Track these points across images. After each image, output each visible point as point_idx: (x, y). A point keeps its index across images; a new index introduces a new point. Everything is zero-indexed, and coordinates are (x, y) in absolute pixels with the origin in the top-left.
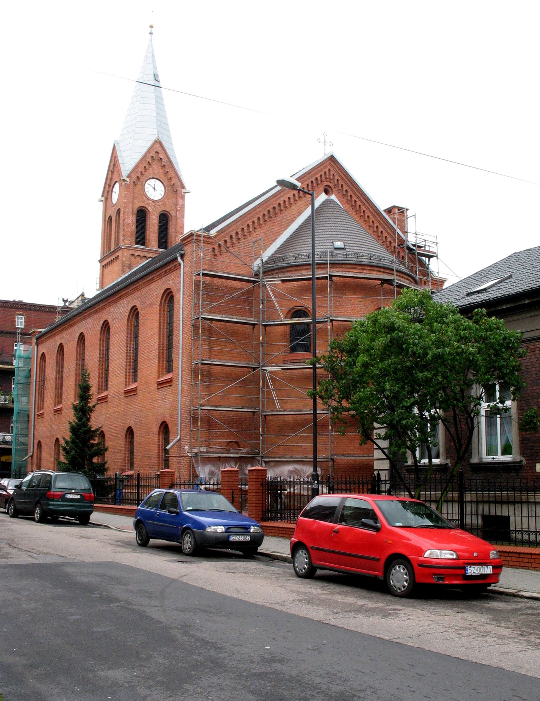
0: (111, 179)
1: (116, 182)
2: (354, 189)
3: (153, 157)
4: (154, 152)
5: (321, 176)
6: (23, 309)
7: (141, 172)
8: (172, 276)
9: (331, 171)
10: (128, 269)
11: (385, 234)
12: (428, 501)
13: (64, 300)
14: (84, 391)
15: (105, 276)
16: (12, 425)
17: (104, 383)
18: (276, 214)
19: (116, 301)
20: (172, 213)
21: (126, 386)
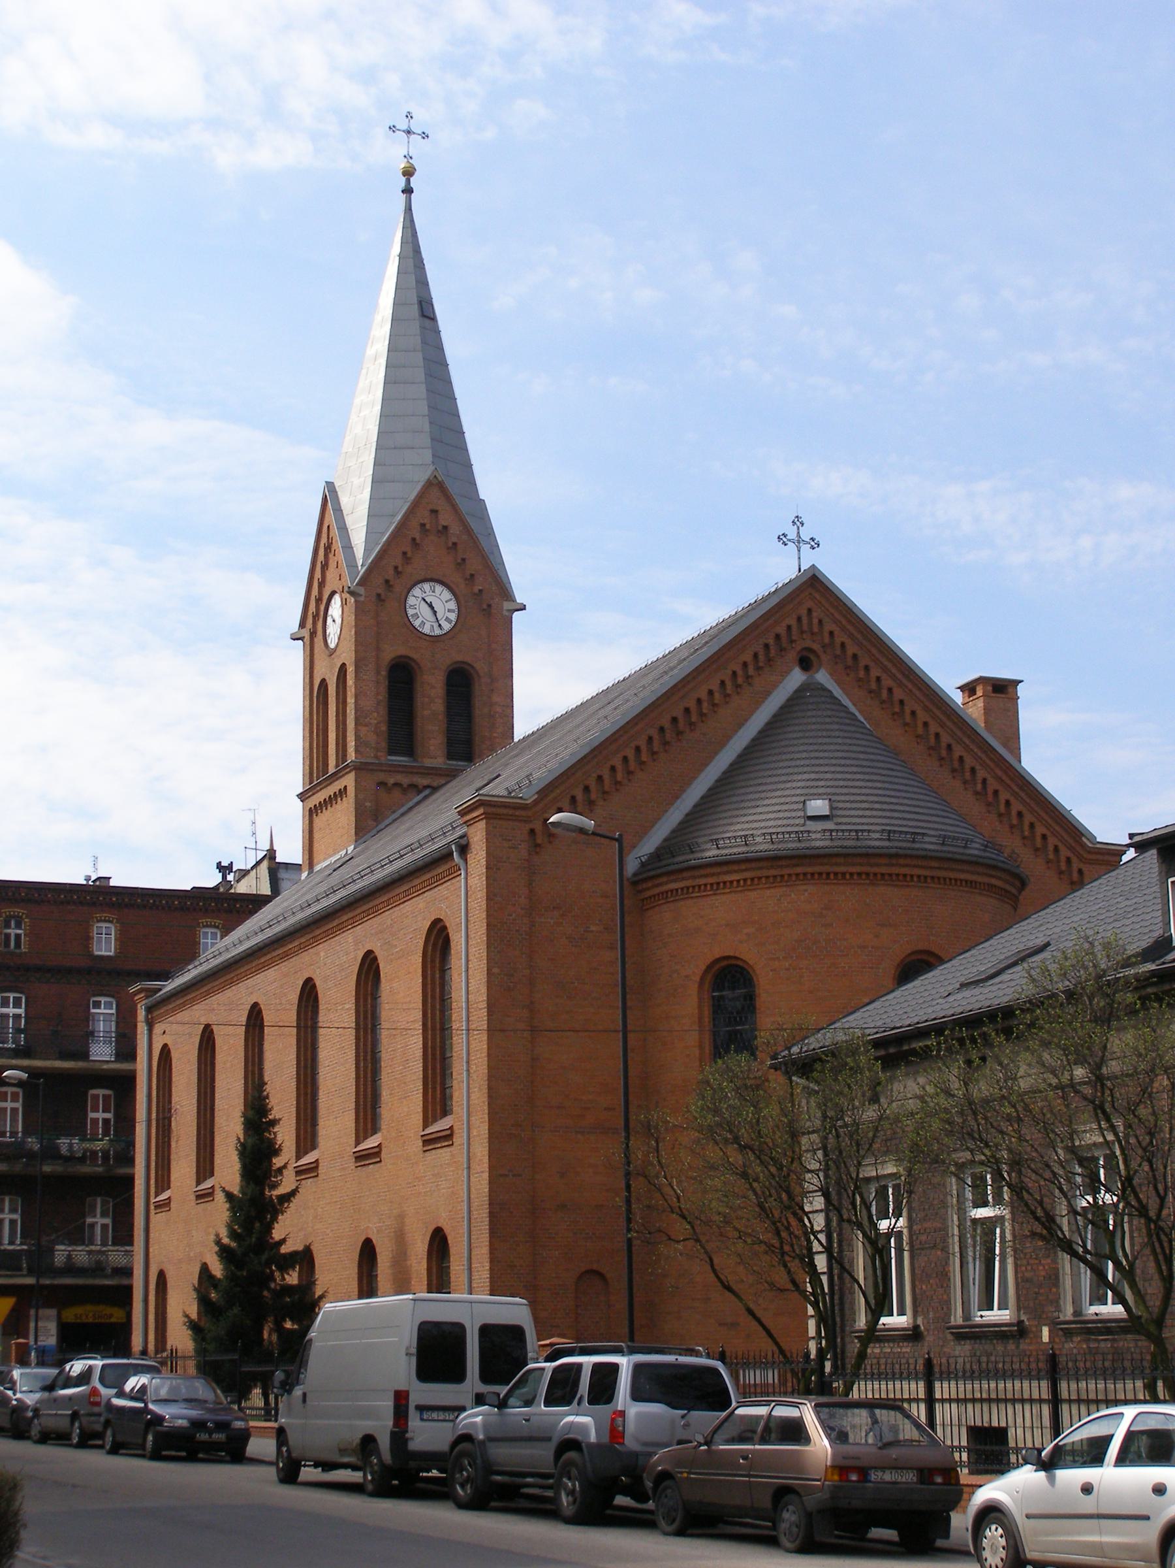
0: (322, 584)
1: (333, 593)
2: (874, 651)
3: (423, 525)
4: (427, 513)
5: (789, 627)
6: (111, 906)
7: (396, 568)
8: (443, 890)
9: (814, 614)
10: (370, 822)
11: (958, 751)
12: (906, 1400)
13: (220, 866)
14: (258, 1156)
15: (316, 836)
16: (89, 1220)
17: (307, 1138)
18: (679, 733)
19: (330, 934)
20: (481, 666)
21: (357, 1143)
